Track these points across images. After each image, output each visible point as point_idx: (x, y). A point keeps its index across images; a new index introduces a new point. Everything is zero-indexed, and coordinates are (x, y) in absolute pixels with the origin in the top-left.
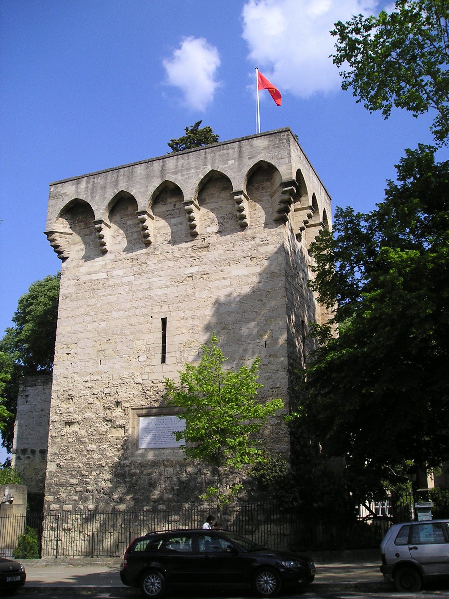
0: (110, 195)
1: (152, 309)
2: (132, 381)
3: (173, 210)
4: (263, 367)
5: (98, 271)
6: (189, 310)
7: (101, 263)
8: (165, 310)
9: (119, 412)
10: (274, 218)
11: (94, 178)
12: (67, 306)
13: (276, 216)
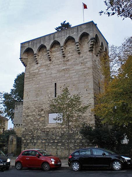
0: (38, 46)
9: (43, 112)
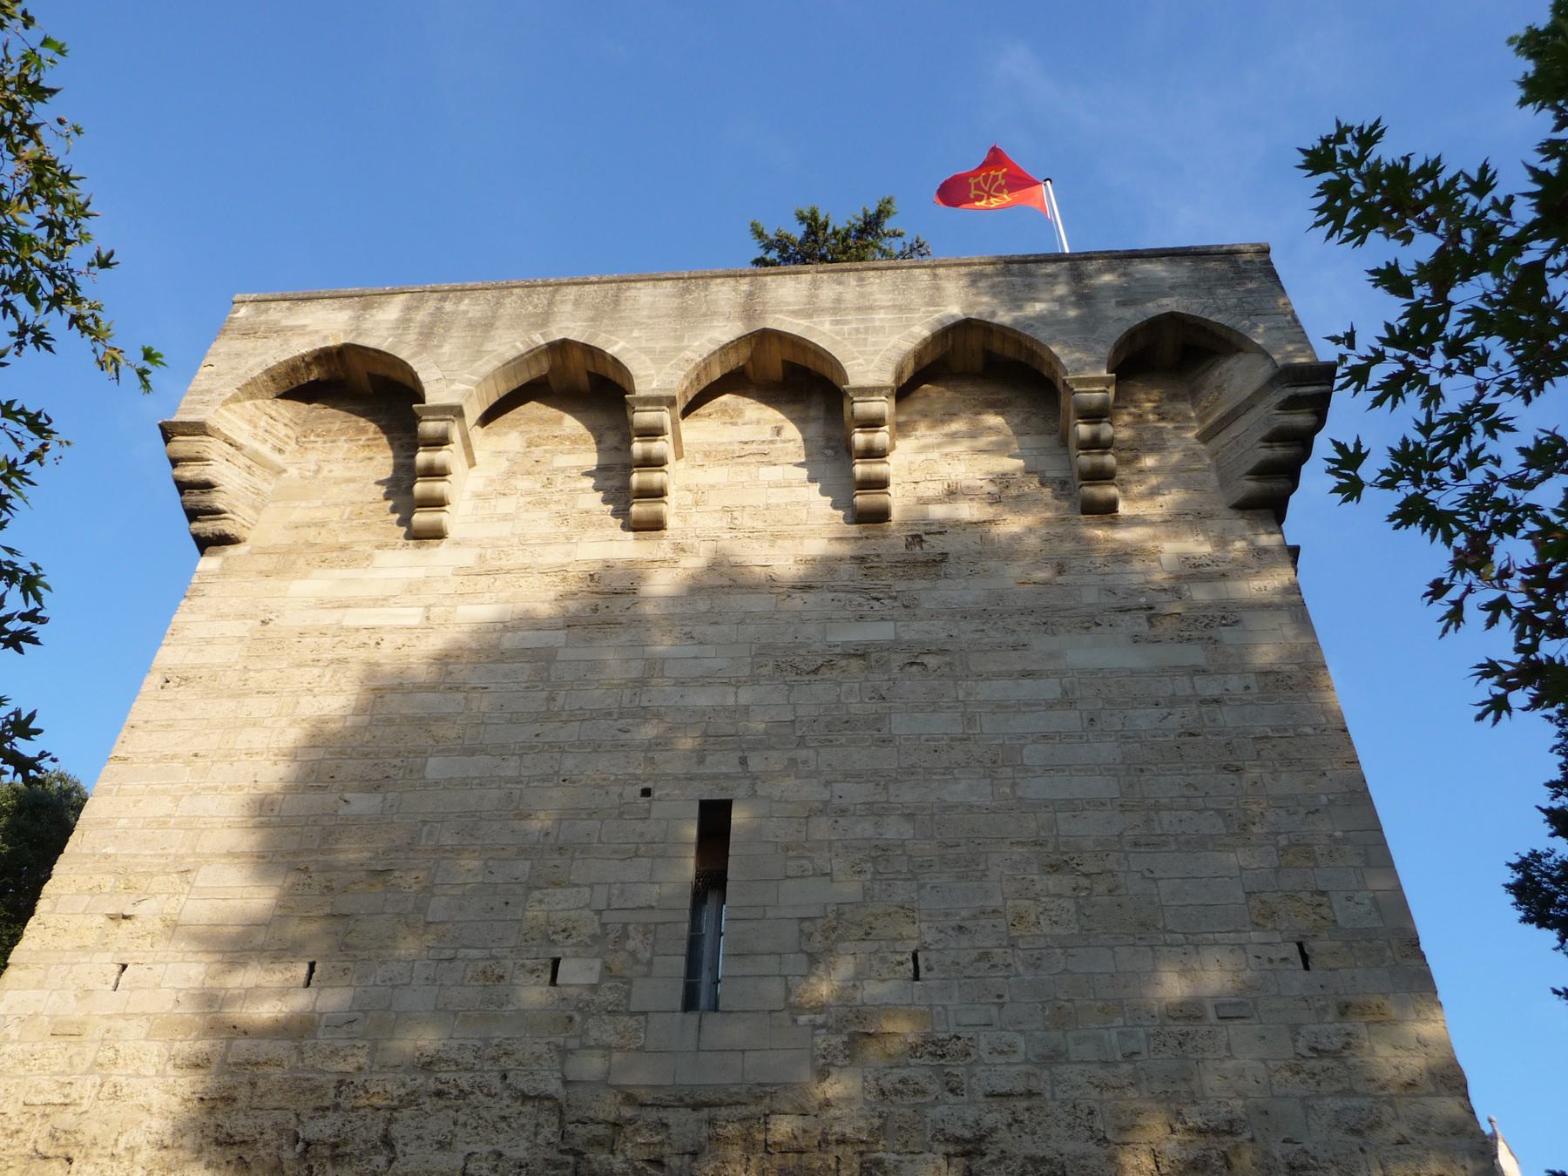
2: (497, 1085)
3: (772, 442)
4: (1314, 1064)
5: (382, 601)
6: (848, 776)
8: (724, 769)
11: (443, 299)
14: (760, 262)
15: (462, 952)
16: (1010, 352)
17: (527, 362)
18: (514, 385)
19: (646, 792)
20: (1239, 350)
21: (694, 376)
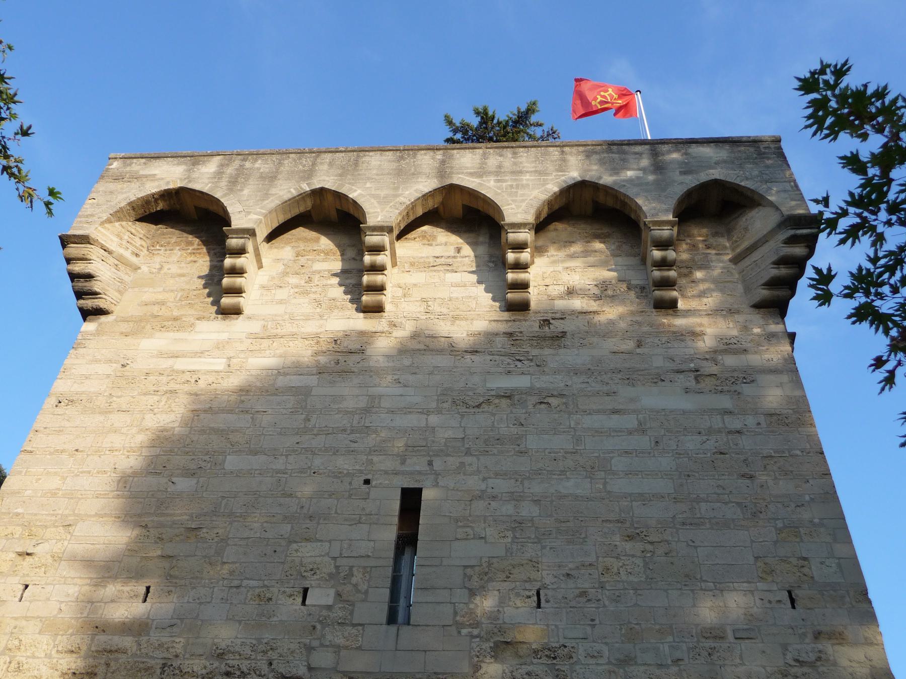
1: (371, 462)
3: (454, 257)
5: (200, 354)
7: (214, 336)
8: (418, 468)
10: (756, 299)
12: (67, 424)
13: (764, 293)
14: (449, 140)
15: (245, 582)
16: (610, 202)
17: (298, 202)
18: (289, 216)
19: (367, 482)
20: (759, 205)
21: (405, 213)
